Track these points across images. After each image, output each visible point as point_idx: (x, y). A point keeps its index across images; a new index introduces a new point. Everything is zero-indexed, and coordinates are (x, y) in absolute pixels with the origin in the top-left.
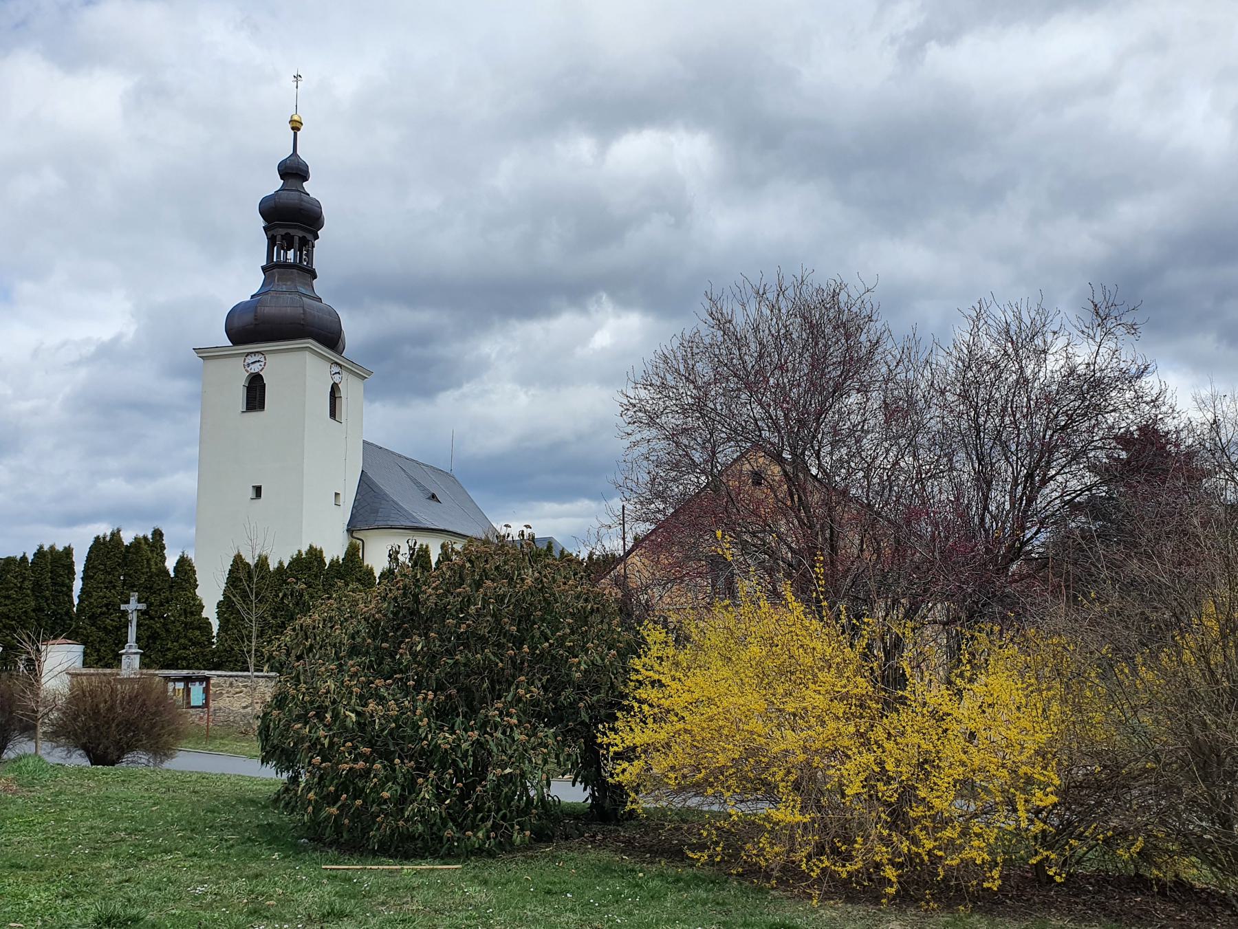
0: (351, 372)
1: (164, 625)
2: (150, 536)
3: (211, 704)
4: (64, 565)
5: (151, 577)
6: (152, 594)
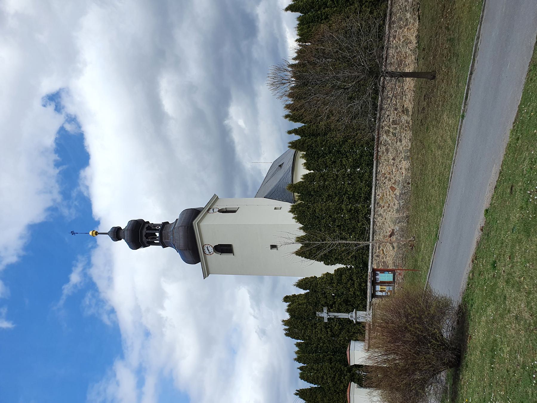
0: (213, 204)
1: (339, 296)
2: (288, 304)
3: (391, 267)
4: (306, 347)
5: (309, 303)
6: (319, 303)
